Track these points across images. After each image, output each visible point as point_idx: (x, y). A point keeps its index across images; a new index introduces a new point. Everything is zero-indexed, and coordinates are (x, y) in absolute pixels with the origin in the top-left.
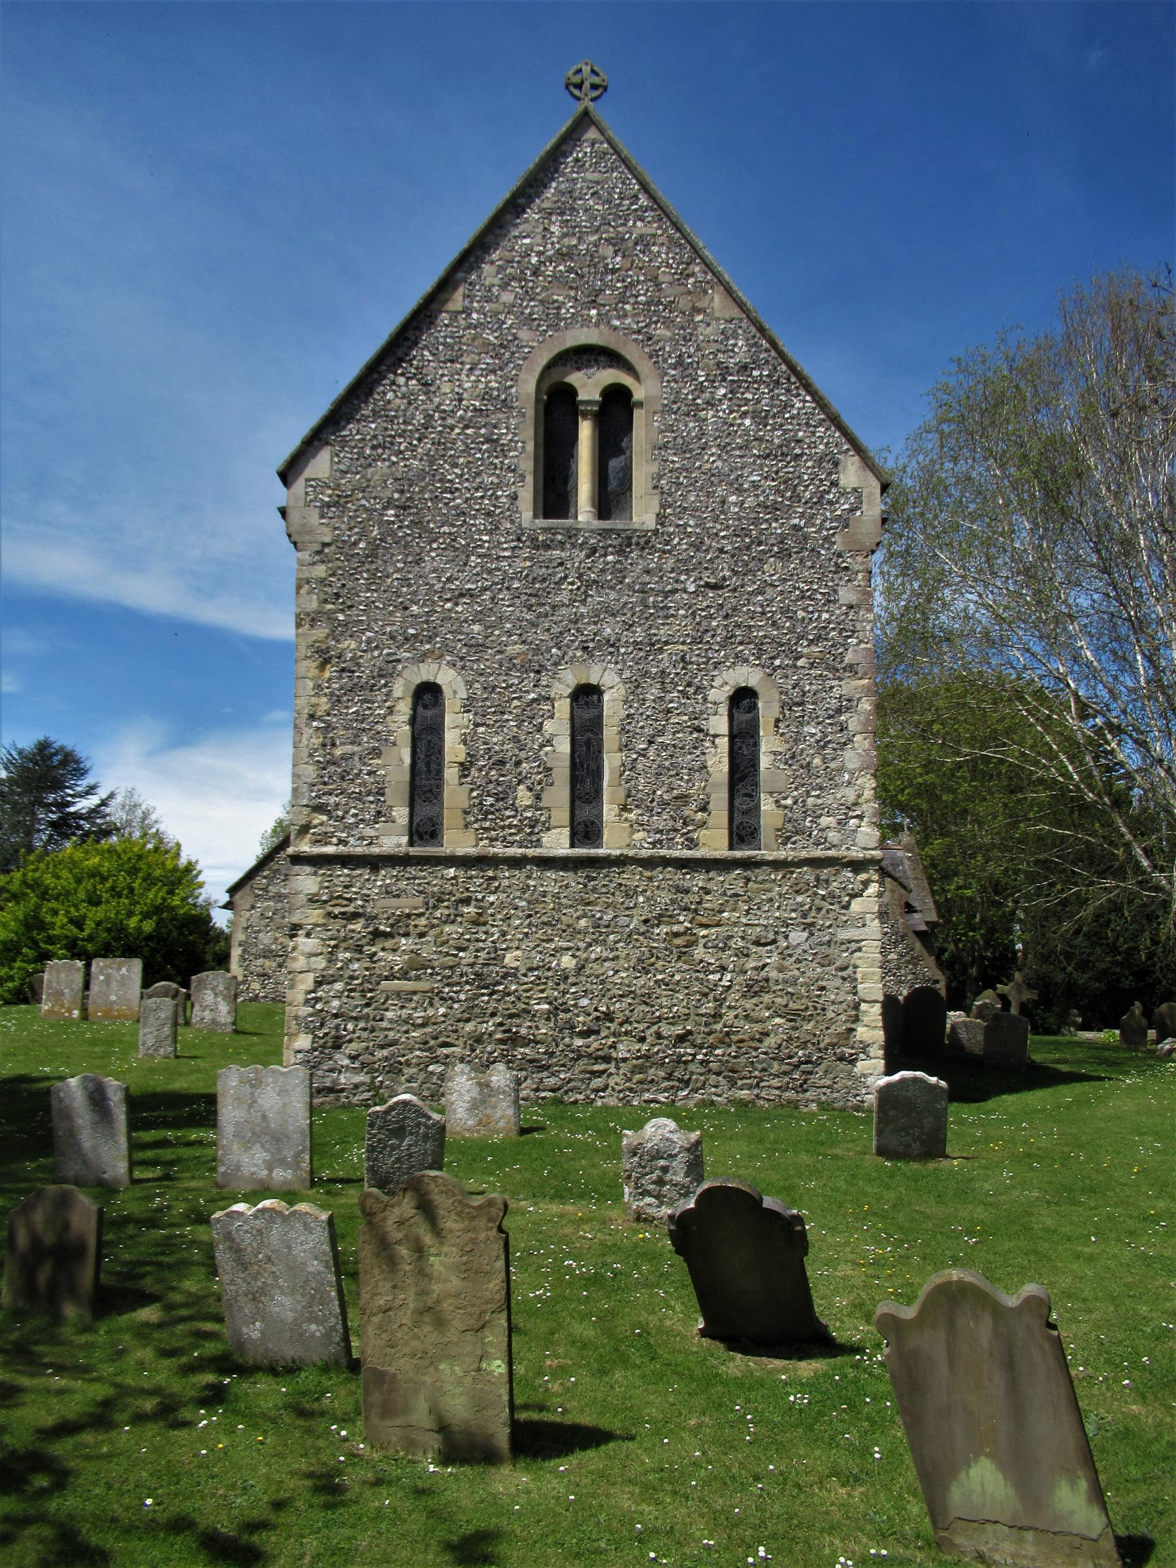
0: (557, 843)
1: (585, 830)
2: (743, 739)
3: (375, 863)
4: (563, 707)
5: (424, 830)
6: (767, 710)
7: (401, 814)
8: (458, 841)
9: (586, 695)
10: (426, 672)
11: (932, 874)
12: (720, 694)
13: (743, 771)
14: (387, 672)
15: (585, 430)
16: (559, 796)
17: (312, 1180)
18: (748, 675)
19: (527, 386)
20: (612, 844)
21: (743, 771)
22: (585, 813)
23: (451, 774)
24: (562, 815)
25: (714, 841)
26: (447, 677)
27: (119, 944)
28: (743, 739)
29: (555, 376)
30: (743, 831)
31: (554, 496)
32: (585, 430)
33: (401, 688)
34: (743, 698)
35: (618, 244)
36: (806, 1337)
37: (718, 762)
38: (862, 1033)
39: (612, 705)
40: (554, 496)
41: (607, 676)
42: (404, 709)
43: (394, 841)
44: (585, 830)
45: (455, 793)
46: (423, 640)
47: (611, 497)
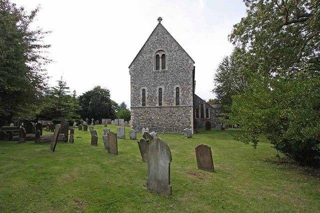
0: (157, 105)
1: (160, 104)
2: (178, 93)
3: (139, 108)
4: (158, 91)
5: (144, 105)
6: (180, 90)
7: (141, 103)
8: (147, 106)
9: (160, 89)
10: (143, 88)
11: (106, 102)
12: (175, 88)
13: (178, 96)
14: (140, 88)
15: (160, 59)
16: (157, 101)
17: (123, 138)
18: (178, 86)
19: (154, 55)
20: (163, 106)
21: (178, 96)
22: (160, 102)
23: (146, 98)
24: (158, 102)
25: (174, 105)
26: (145, 88)
27: (122, 118)
28: (178, 93)
29: (157, 54)
30: (178, 103)
31: (157, 68)
32: (160, 59)
33: (158, 89)
34: (177, 88)
35: (163, 38)
36: (211, 168)
37: (175, 96)
38: (191, 126)
39: (163, 91)
40: (157, 68)
41: (163, 87)
42: (141, 92)
43: (141, 106)
44: (160, 104)
45: (147, 100)
46: (143, 84)
47: (164, 67)
